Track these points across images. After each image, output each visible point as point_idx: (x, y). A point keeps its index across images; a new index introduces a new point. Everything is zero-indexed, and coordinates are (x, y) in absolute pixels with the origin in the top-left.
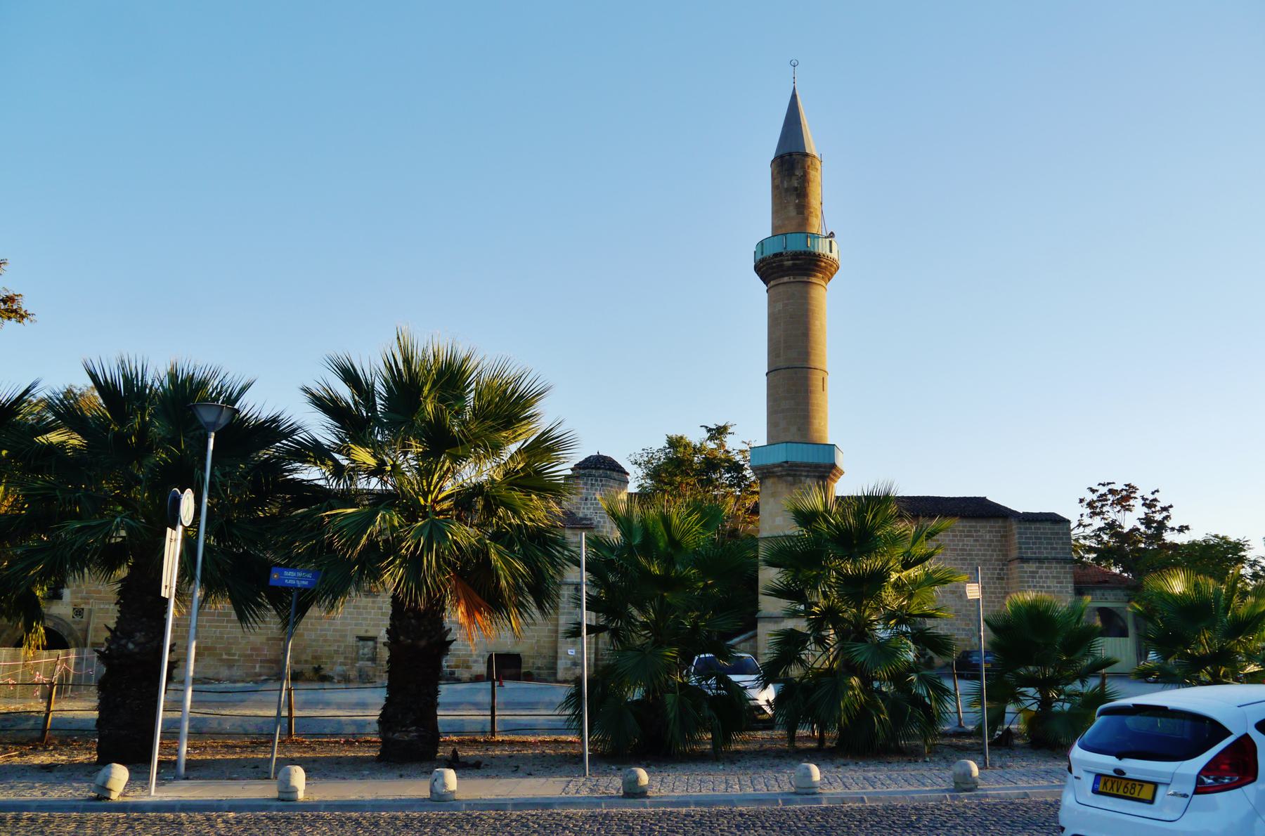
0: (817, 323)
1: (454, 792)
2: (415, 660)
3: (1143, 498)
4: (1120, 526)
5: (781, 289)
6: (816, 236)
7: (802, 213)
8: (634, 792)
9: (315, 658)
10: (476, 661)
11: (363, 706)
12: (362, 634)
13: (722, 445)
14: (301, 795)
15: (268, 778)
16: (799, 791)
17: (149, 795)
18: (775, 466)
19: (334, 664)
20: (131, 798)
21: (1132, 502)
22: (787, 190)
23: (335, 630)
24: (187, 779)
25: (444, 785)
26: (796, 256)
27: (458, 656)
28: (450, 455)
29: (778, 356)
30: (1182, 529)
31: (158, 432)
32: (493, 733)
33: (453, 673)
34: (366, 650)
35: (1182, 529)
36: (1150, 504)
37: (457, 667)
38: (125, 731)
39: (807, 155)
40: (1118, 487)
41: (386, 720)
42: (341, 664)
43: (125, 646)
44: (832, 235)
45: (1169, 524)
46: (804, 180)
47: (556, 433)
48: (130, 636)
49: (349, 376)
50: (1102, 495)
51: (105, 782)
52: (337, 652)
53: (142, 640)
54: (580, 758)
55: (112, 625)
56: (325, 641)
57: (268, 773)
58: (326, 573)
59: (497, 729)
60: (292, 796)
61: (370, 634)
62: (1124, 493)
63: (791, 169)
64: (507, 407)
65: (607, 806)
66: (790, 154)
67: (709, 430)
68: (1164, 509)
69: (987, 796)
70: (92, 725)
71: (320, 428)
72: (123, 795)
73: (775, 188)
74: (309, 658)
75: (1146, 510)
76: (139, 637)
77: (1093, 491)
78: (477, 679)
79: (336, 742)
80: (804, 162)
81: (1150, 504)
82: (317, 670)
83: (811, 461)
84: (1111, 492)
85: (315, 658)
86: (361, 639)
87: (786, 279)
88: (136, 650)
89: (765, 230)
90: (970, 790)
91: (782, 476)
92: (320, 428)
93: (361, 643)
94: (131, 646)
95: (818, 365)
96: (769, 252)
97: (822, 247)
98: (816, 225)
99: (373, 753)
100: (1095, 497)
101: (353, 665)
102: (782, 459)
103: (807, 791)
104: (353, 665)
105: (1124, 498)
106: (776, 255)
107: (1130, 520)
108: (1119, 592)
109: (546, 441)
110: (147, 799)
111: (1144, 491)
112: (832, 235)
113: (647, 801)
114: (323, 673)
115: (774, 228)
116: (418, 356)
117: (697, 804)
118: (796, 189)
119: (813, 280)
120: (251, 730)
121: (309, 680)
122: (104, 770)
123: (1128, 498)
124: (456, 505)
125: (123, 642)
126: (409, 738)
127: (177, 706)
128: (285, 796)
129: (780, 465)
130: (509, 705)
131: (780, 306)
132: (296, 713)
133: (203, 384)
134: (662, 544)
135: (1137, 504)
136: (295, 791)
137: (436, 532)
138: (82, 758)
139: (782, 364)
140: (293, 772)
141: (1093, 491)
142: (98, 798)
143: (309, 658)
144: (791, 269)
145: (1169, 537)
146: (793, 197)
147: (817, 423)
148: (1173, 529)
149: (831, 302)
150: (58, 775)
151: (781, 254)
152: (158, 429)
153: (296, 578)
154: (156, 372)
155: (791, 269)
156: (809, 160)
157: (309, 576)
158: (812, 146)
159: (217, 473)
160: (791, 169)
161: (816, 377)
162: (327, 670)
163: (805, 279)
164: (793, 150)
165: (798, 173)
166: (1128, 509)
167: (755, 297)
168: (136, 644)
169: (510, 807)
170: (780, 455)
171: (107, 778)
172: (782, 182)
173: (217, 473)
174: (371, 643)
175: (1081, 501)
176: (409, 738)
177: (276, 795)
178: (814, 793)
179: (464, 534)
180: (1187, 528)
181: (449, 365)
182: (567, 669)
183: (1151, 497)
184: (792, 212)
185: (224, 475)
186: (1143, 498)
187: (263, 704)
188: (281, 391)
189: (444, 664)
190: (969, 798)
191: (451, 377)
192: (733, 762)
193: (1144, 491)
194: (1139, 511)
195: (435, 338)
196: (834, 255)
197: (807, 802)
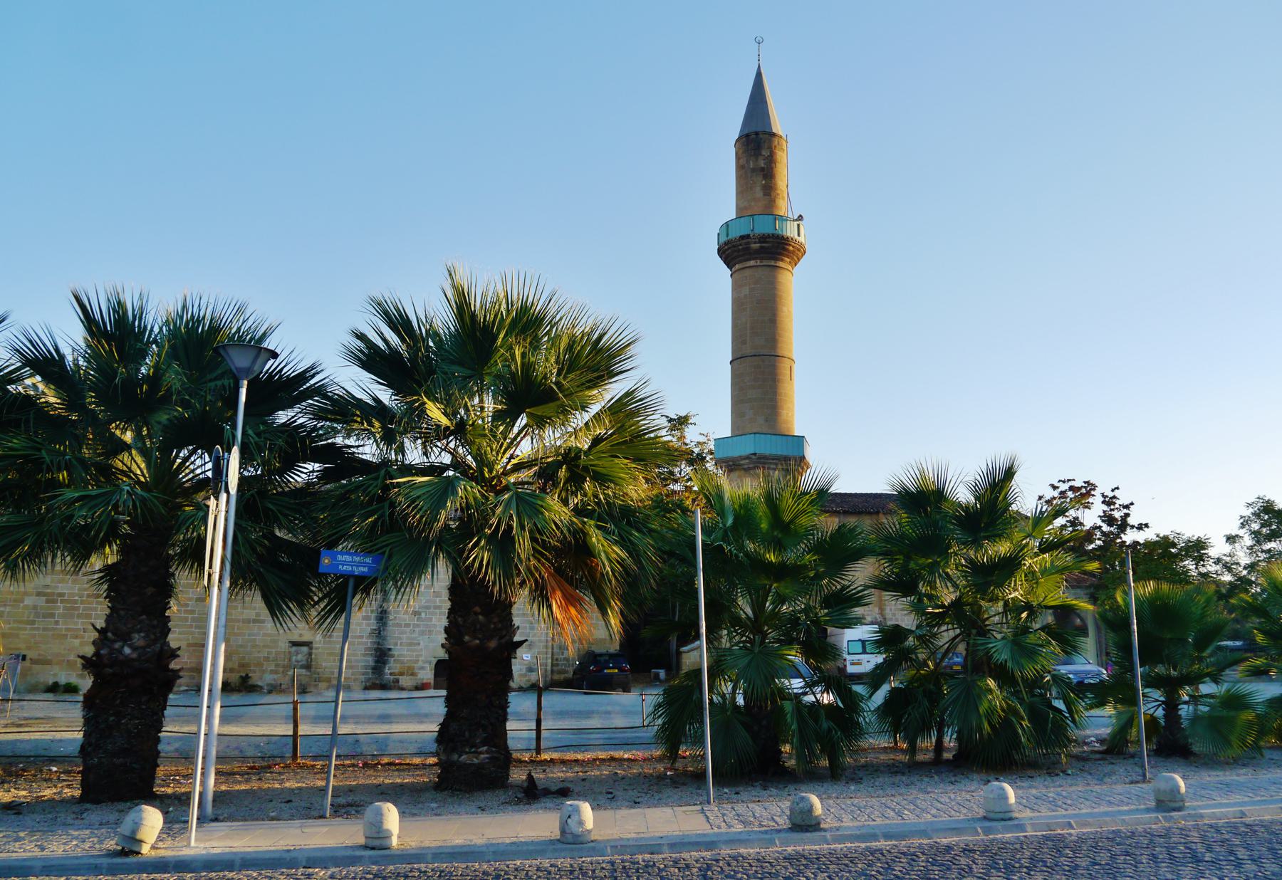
0: (785, 309)
1: (589, 831)
2: (476, 669)
3: (1103, 495)
4: (1082, 524)
5: (747, 272)
6: (784, 219)
7: (769, 195)
8: (804, 824)
9: (242, 666)
10: (422, 668)
11: (418, 721)
12: (296, 638)
13: (682, 437)
14: (395, 841)
15: (322, 817)
16: (992, 815)
17: (188, 845)
18: (742, 458)
19: (264, 672)
20: (169, 851)
21: (1091, 500)
22: (753, 170)
23: (265, 635)
24: (216, 820)
25: (581, 823)
26: (763, 238)
27: (402, 662)
28: (530, 415)
29: (744, 342)
30: (1141, 527)
31: (182, 372)
32: (538, 750)
33: (398, 681)
34: (299, 657)
35: (1141, 527)
36: (1109, 501)
37: (402, 674)
38: (121, 762)
39: (774, 135)
40: (1078, 484)
41: (446, 736)
42: (272, 672)
43: (120, 651)
44: (800, 218)
45: (1130, 521)
46: (771, 160)
47: (641, 394)
48: (125, 638)
49: (399, 323)
50: (1062, 493)
51: (134, 832)
52: (267, 659)
53: (141, 643)
54: (700, 777)
55: (100, 624)
56: (254, 646)
57: (323, 808)
58: (390, 557)
59: (543, 745)
60: (384, 843)
61: (305, 639)
62: (1084, 491)
63: (757, 148)
64: (596, 360)
65: (782, 844)
66: (757, 133)
67: (670, 420)
68: (1127, 507)
69: (1202, 816)
70: (74, 749)
71: (360, 384)
72: (153, 847)
73: (740, 168)
74: (236, 666)
75: (1105, 508)
76: (138, 639)
77: (1055, 488)
78: (422, 687)
79: (353, 765)
80: (770, 142)
81: (1109, 501)
82: (245, 679)
83: (774, 453)
84: (1072, 488)
85: (242, 666)
86: (295, 644)
87: (752, 263)
88: (134, 656)
89: (731, 214)
90: (1179, 809)
91: (750, 469)
92: (360, 384)
93: (294, 649)
94: (127, 650)
95: (785, 353)
96: (735, 234)
97: (790, 231)
98: (782, 208)
99: (425, 778)
100: (1056, 494)
101: (284, 673)
102: (748, 450)
103: (999, 816)
104: (284, 673)
105: (1083, 494)
106: (742, 237)
107: (1091, 517)
108: (1078, 591)
109: (626, 404)
110: (186, 852)
111: (1104, 487)
112: (800, 218)
113: (828, 835)
114: (251, 682)
115: (739, 209)
116: (476, 305)
117: (887, 836)
118: (762, 170)
119: (781, 264)
120: (250, 752)
121: (239, 691)
122: (130, 818)
123: (1088, 494)
124: (539, 475)
125: (117, 645)
126: (472, 761)
127: (203, 726)
128: (376, 843)
129: (747, 457)
130: (561, 714)
131: (746, 290)
132: (303, 729)
133: (215, 329)
134: (764, 526)
135: (1096, 501)
136: (388, 836)
137: (528, 505)
138: (68, 793)
139: (748, 351)
140: (385, 811)
141: (1055, 488)
142: (124, 853)
143: (236, 666)
144: (757, 252)
145: (1129, 537)
146: (760, 178)
147: (784, 413)
148: (1133, 527)
149: (799, 286)
150: (38, 817)
151: (748, 236)
152: (174, 378)
153: (351, 563)
154: (159, 307)
155: (757, 252)
156: (776, 140)
157: (369, 560)
158: (778, 126)
159: (250, 432)
160: (757, 148)
161: (785, 364)
162: (255, 679)
163: (772, 263)
164: (759, 129)
165: (765, 153)
166: (1087, 506)
167: (719, 281)
168: (134, 649)
169: (665, 848)
170: (746, 447)
171: (137, 825)
172: (748, 162)
173: (250, 432)
174: (305, 649)
175: (1040, 498)
176: (472, 761)
177: (362, 841)
178: (1011, 819)
179: (558, 511)
180: (1146, 526)
181: (524, 309)
182: (521, 675)
183: (1111, 494)
184: (759, 193)
185: (258, 435)
186: (1103, 495)
187: (269, 719)
188: (317, 340)
189: (387, 671)
190: (1184, 818)
191: (527, 322)
192: (858, 781)
193: (1104, 487)
194: (1098, 507)
195: (490, 283)
196: (801, 239)
197: (1008, 830)
